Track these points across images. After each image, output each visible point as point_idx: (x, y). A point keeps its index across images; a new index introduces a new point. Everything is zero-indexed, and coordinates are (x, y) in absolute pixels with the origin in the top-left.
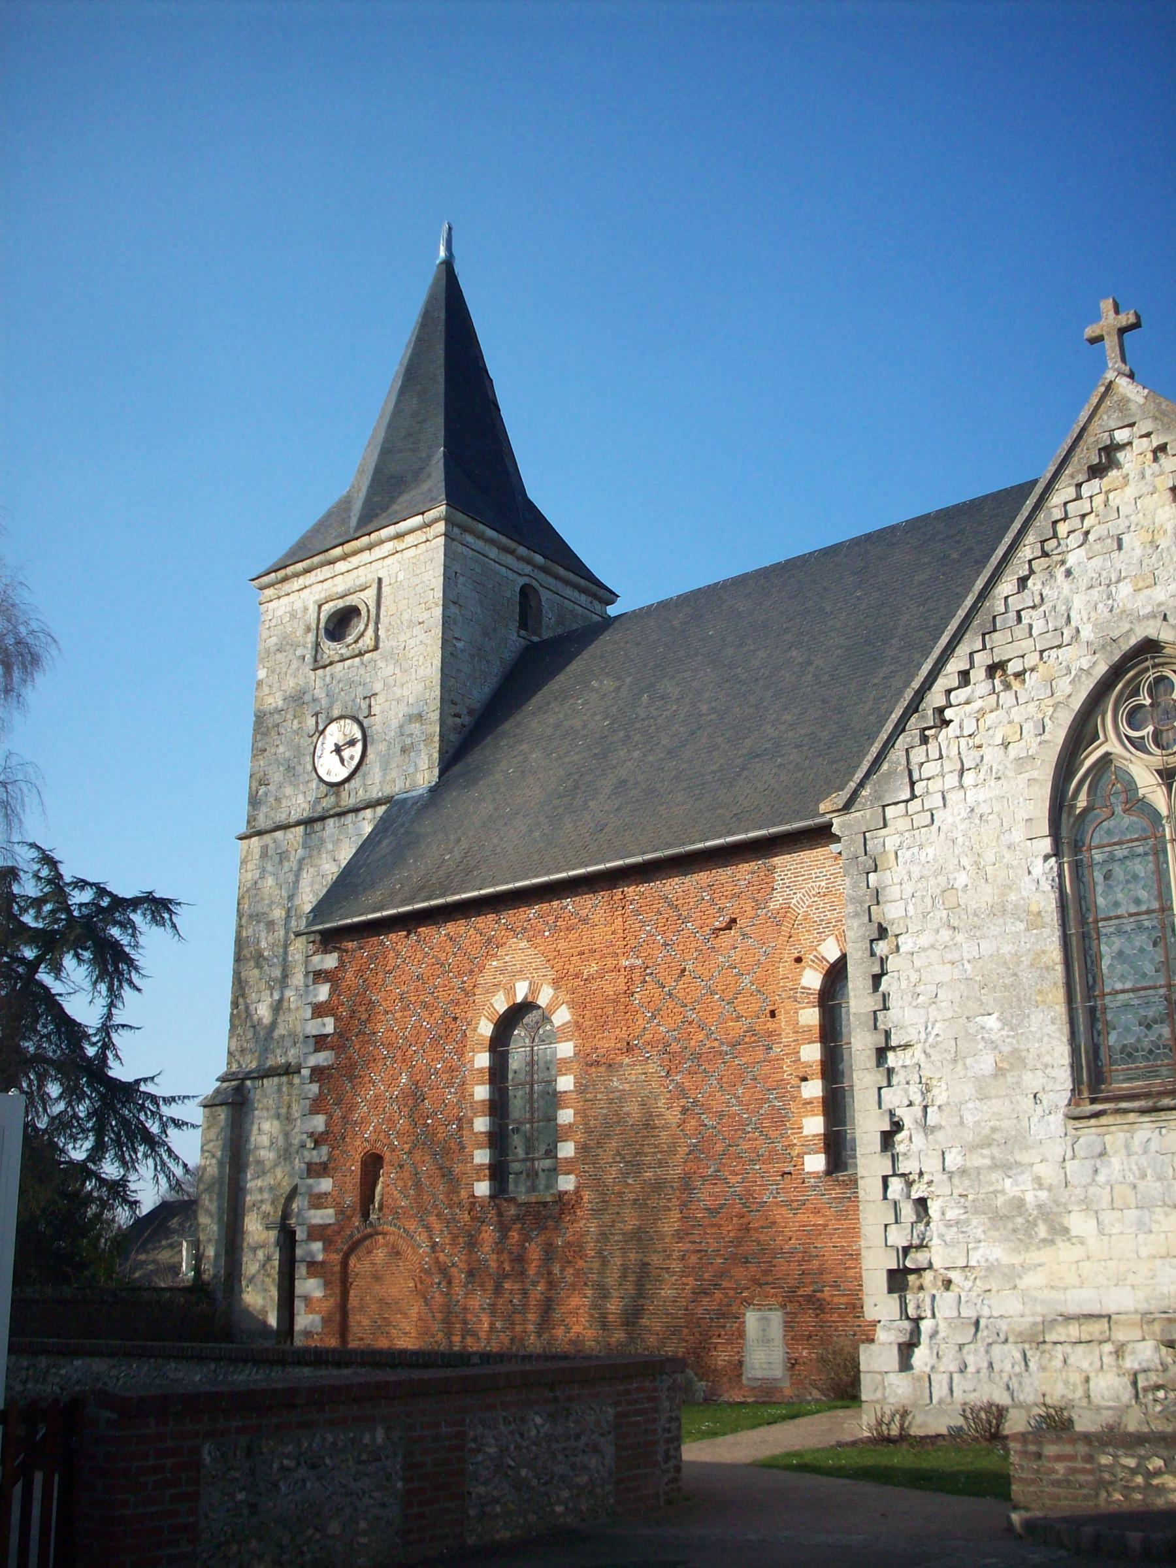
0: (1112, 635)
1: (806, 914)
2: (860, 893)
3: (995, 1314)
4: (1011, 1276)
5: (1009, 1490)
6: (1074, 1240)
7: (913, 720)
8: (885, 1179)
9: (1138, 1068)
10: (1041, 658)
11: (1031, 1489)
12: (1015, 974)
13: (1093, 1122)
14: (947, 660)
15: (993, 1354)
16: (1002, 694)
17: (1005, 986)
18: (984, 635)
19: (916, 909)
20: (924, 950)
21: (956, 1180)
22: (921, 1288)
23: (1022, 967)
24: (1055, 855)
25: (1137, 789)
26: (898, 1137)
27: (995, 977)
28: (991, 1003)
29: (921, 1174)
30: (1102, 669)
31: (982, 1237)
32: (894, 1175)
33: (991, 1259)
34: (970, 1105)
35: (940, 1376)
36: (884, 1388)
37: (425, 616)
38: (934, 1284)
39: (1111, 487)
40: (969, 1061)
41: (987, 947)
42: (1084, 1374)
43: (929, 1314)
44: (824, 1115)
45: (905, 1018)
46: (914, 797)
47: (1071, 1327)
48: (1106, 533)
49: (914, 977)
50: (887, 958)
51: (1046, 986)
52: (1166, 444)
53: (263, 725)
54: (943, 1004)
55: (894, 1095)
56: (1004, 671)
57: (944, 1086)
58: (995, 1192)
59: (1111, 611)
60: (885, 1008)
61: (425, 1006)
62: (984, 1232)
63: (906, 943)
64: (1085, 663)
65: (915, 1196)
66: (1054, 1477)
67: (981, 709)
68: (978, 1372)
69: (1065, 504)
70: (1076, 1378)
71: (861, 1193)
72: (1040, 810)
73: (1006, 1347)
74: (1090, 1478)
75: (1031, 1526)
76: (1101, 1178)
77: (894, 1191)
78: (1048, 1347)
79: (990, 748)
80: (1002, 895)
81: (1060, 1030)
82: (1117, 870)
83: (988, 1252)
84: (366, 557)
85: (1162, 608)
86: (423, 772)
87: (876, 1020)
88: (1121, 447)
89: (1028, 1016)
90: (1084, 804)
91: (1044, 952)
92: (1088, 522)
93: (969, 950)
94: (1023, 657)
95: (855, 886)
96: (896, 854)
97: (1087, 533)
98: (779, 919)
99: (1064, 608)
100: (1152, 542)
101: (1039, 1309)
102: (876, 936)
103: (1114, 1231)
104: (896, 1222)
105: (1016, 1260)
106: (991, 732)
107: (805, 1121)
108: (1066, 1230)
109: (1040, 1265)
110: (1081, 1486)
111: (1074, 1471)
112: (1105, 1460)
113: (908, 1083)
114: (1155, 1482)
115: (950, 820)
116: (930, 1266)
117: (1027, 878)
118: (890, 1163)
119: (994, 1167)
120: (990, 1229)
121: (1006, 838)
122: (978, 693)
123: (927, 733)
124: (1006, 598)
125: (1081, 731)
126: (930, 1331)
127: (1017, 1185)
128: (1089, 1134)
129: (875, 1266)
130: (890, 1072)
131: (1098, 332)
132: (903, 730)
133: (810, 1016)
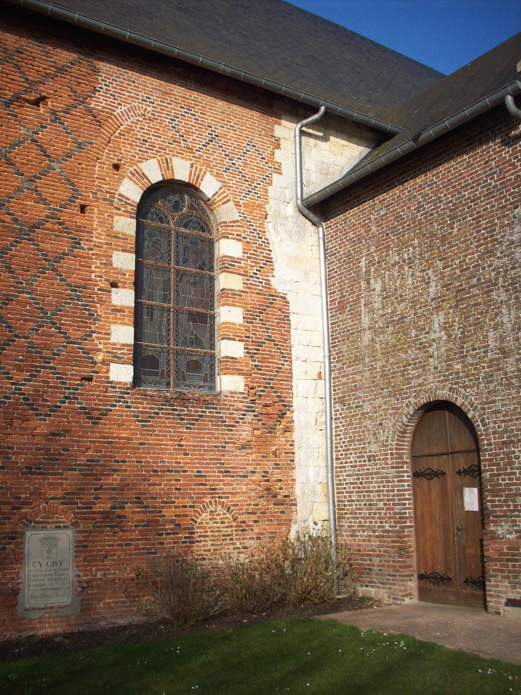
1: (129, 130)
98: (97, 119)
107: (114, 328)
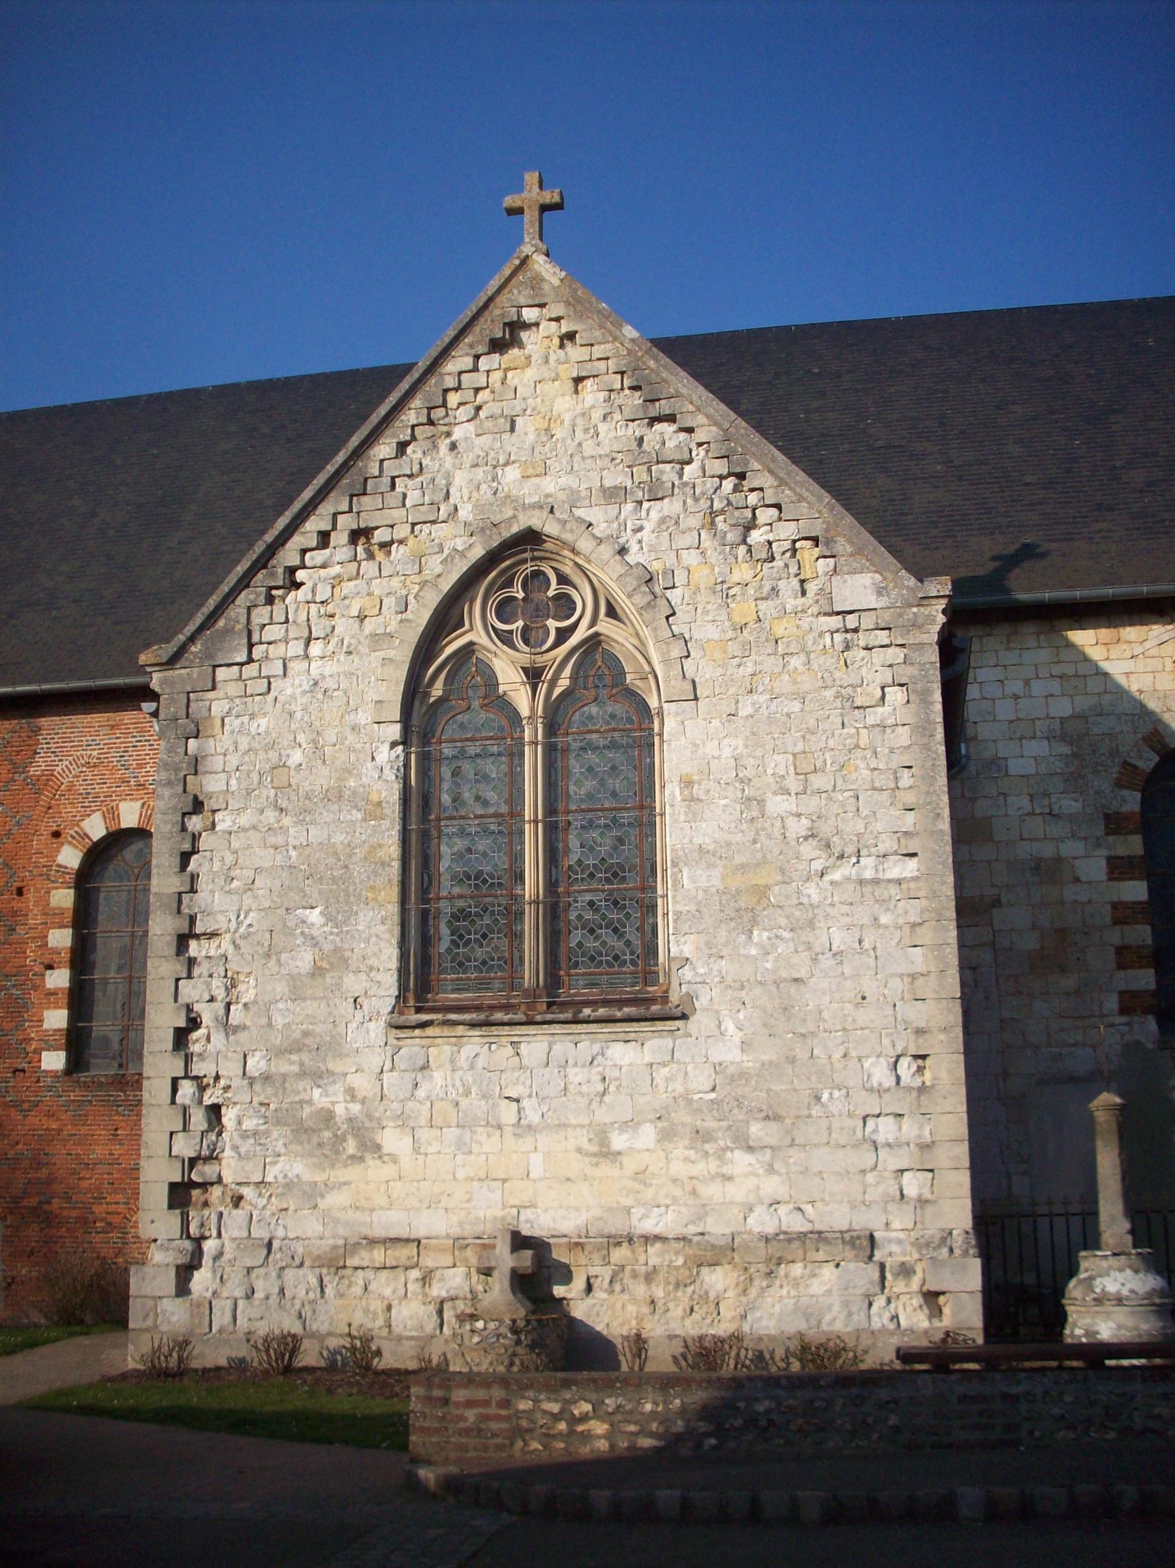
0: (492, 519)
2: (177, 759)
3: (291, 1235)
4: (312, 1194)
5: (408, 1441)
6: (386, 1158)
7: (260, 576)
8: (175, 1082)
9: (469, 979)
10: (413, 531)
11: (434, 1439)
12: (346, 867)
13: (417, 1032)
14: (308, 517)
15: (285, 1279)
16: (364, 563)
17: (333, 878)
18: (352, 496)
19: (239, 784)
20: (245, 830)
21: (257, 1087)
22: (206, 1204)
23: (354, 859)
24: (403, 743)
25: (498, 684)
26: (195, 1035)
27: (322, 868)
28: (315, 895)
29: (217, 1078)
30: (478, 552)
31: (283, 1150)
32: (186, 1077)
33: (290, 1175)
34: (281, 1005)
35: (223, 1303)
36: (157, 1315)
38: (222, 1201)
39: (512, 365)
40: (284, 956)
41: (316, 834)
42: (386, 1302)
43: (214, 1233)
44: (69, 1009)
45: (215, 903)
46: (250, 660)
47: (375, 1252)
48: (499, 411)
49: (229, 859)
50: (200, 835)
51: (379, 882)
52: (576, 332)
54: (260, 892)
55: (194, 987)
56: (368, 539)
57: (252, 982)
58: (301, 1102)
59: (495, 494)
60: (193, 890)
62: (285, 1145)
63: (224, 821)
64: (460, 544)
65: (208, 1100)
66: (462, 1425)
67: (338, 576)
68: (267, 1298)
69: (460, 373)
70: (378, 1306)
71: (146, 1096)
72: (394, 694)
73: (301, 1272)
74: (505, 1425)
75: (452, 1485)
76: (421, 1093)
77: (184, 1096)
78: (348, 1272)
79: (344, 620)
80: (340, 779)
81: (390, 931)
82: (467, 767)
83: (288, 1167)
85: (550, 500)
87: (180, 902)
88: (526, 326)
89: (356, 913)
90: (440, 693)
91: (380, 846)
92: (482, 396)
94: (392, 526)
95: (171, 750)
96: (223, 721)
97: (479, 408)
99: (444, 482)
100: (547, 430)
101: (341, 1231)
102: (189, 809)
103: (431, 1150)
104: (184, 1130)
105: (319, 1177)
106: (347, 602)
107: (46, 1013)
108: (378, 1147)
109: (345, 1184)
110: (493, 1435)
111: (488, 1418)
112: (524, 1405)
113: (211, 976)
114: (580, 1428)
115: (289, 691)
116: (220, 1180)
117: (369, 765)
118: (182, 1064)
119: (303, 1074)
120: (291, 1142)
121: (350, 719)
122: (337, 558)
123: (274, 592)
124: (382, 461)
125: (446, 614)
126: (214, 1252)
127: (327, 1095)
128: (412, 1046)
129: (157, 1175)
130: (192, 962)
131: (518, 204)
132: (248, 586)
133: (64, 898)
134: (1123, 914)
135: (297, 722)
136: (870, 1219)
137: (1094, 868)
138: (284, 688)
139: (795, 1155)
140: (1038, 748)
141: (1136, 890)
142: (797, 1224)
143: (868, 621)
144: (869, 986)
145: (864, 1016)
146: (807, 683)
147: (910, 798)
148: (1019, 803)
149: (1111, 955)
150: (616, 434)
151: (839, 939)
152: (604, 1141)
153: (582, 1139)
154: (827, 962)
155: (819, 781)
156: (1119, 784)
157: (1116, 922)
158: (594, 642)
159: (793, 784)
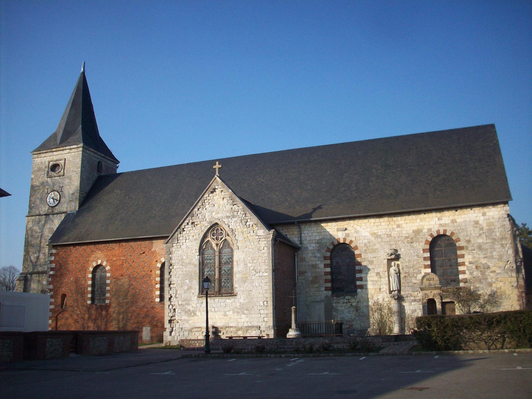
4: (187, 321)
30: (209, 226)
37: (76, 170)
41: (187, 269)
45: (174, 279)
53: (33, 188)
61: (77, 263)
63: (175, 267)
84: (61, 152)
86: (74, 207)
93: (185, 269)
133: (158, 272)
134: (326, 273)
135: (184, 252)
136: (260, 324)
137: (322, 266)
138: (183, 247)
139: (250, 315)
140: (314, 245)
141: (328, 270)
142: (250, 325)
143: (262, 237)
144: (261, 291)
145: (260, 296)
146: (254, 247)
147: (266, 264)
148: (310, 255)
149: (324, 280)
150: (229, 207)
151: (257, 285)
152: (225, 313)
153: (223, 313)
154: (255, 288)
155: (255, 261)
156: (326, 251)
157: (325, 275)
158: (225, 240)
159: (251, 262)
